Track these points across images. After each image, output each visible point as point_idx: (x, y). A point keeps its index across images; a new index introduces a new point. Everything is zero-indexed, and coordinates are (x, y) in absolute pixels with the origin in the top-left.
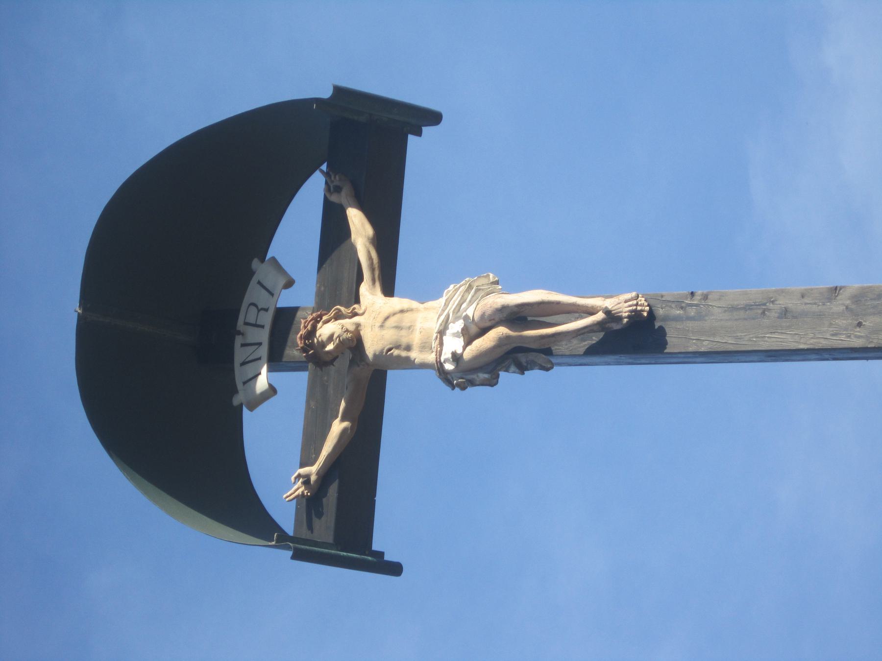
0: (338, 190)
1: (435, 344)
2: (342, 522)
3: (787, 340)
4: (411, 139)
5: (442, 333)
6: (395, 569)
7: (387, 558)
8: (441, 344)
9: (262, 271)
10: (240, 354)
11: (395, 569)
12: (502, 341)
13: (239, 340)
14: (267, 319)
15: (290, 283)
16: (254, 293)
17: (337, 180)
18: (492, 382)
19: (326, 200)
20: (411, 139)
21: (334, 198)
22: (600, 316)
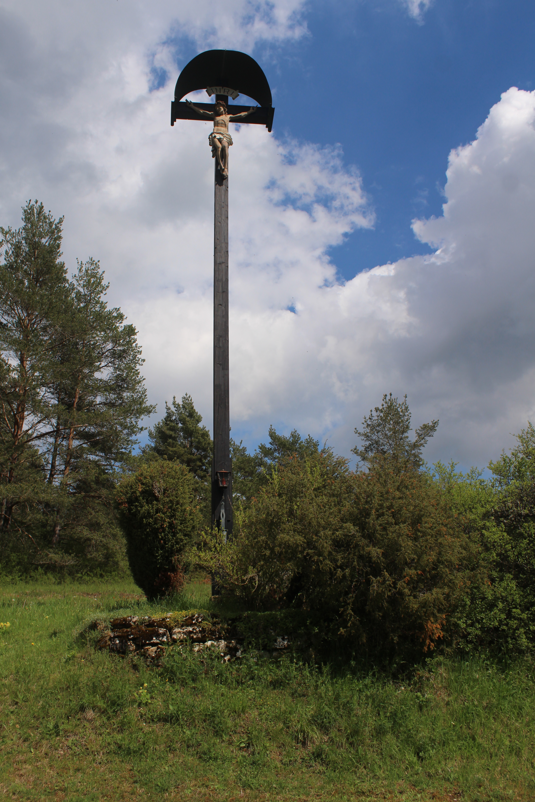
0: (253, 109)
1: (218, 132)
2: (181, 111)
3: (217, 208)
4: (265, 125)
5: (220, 133)
6: (172, 124)
7: (173, 100)
8: (218, 133)
9: (236, 92)
10: (218, 88)
11: (172, 124)
12: (219, 148)
13: (221, 88)
14: (226, 94)
15: (234, 99)
16: (231, 91)
17: (255, 109)
18: (210, 145)
19: (250, 107)
20: (265, 125)
21: (251, 108)
22: (223, 168)
